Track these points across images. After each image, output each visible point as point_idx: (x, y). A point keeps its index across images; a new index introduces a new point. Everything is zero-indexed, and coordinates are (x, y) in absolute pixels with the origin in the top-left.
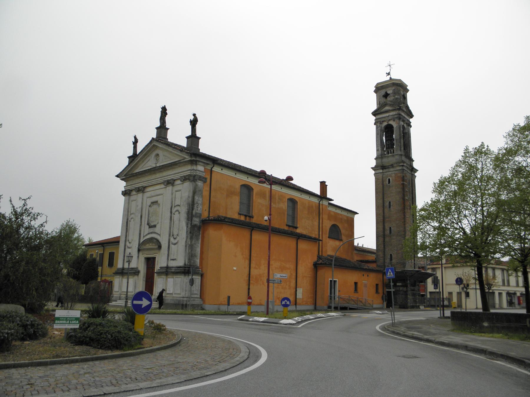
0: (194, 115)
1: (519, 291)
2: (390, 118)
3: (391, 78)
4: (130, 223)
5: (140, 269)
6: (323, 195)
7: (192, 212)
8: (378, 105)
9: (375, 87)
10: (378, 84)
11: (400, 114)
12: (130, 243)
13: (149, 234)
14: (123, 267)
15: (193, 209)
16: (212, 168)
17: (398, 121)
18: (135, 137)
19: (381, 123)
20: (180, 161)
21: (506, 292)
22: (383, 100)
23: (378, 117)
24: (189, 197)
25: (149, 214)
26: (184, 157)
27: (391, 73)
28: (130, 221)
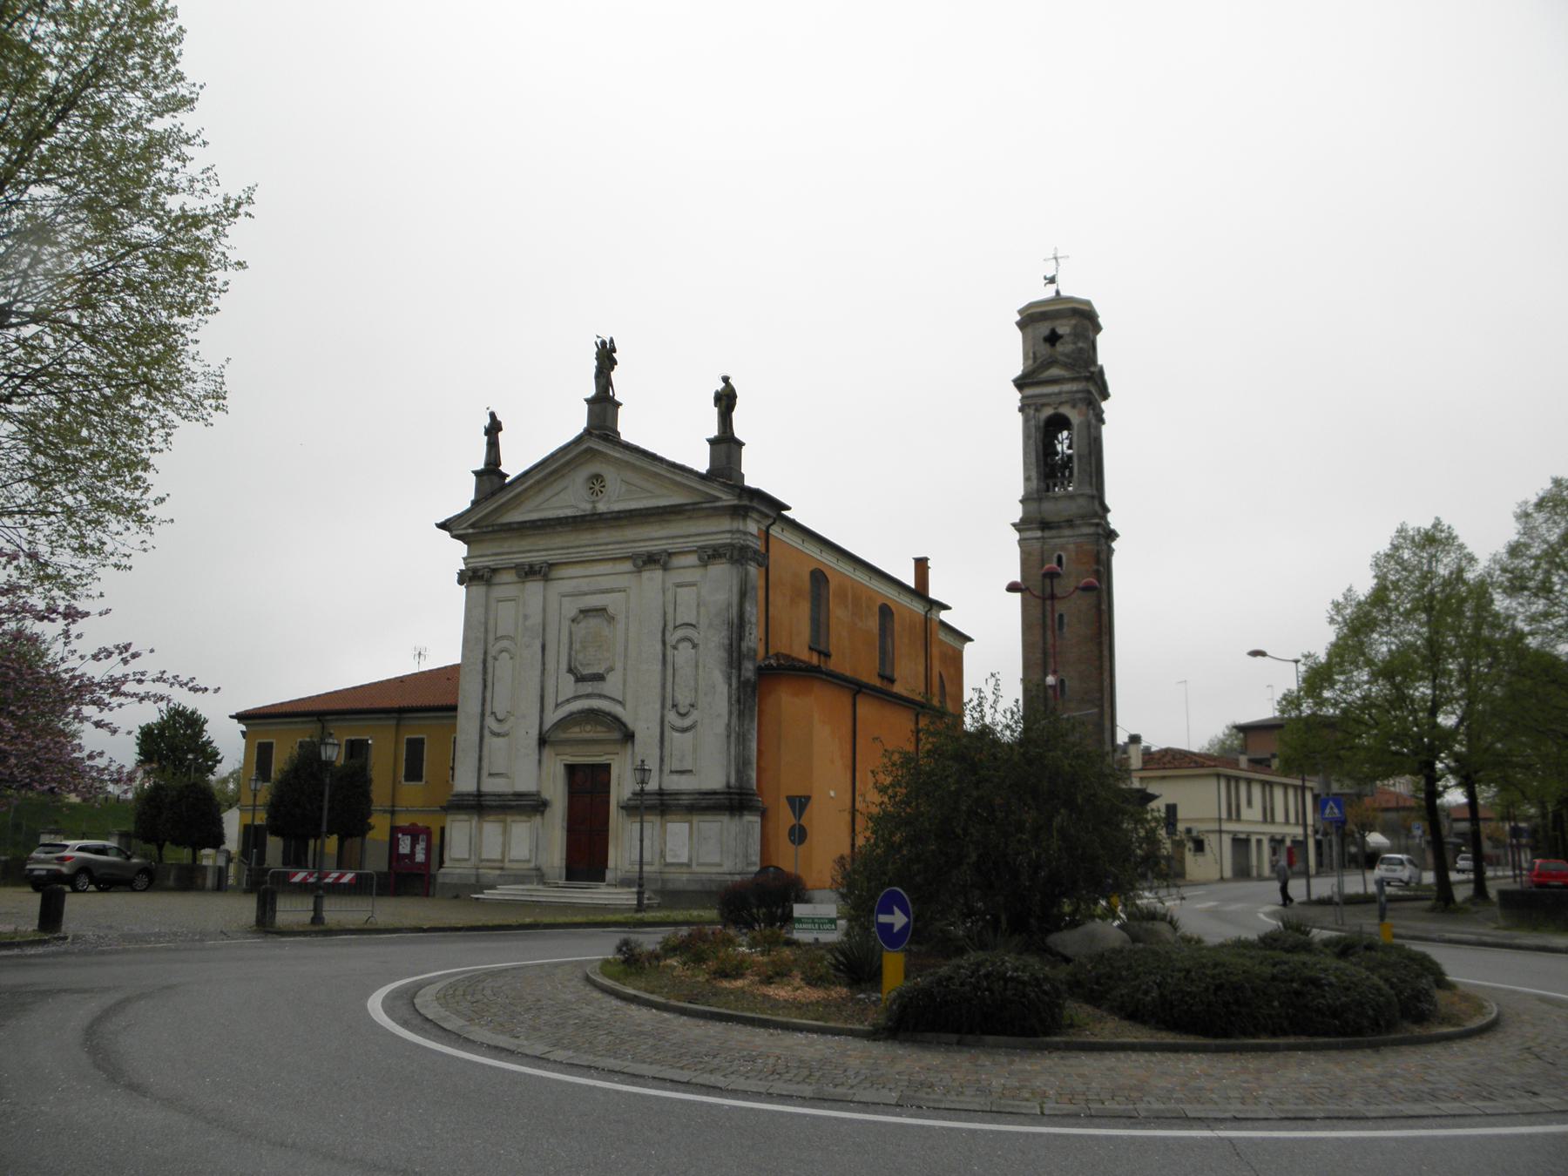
0: (726, 380)
1: (1289, 834)
2: (1064, 398)
3: (1058, 292)
4: (497, 663)
5: (546, 795)
6: (920, 591)
7: (739, 647)
8: (1030, 362)
9: (1020, 312)
10: (1031, 305)
11: (1089, 392)
12: (499, 721)
13: (577, 698)
14: (479, 790)
15: (741, 638)
16: (768, 528)
17: (1084, 408)
18: (493, 415)
19: (1037, 410)
20: (700, 506)
21: (1268, 837)
22: (1044, 349)
23: (1029, 391)
24: (730, 605)
25: (571, 643)
26: (707, 494)
27: (1058, 279)
28: (495, 659)
